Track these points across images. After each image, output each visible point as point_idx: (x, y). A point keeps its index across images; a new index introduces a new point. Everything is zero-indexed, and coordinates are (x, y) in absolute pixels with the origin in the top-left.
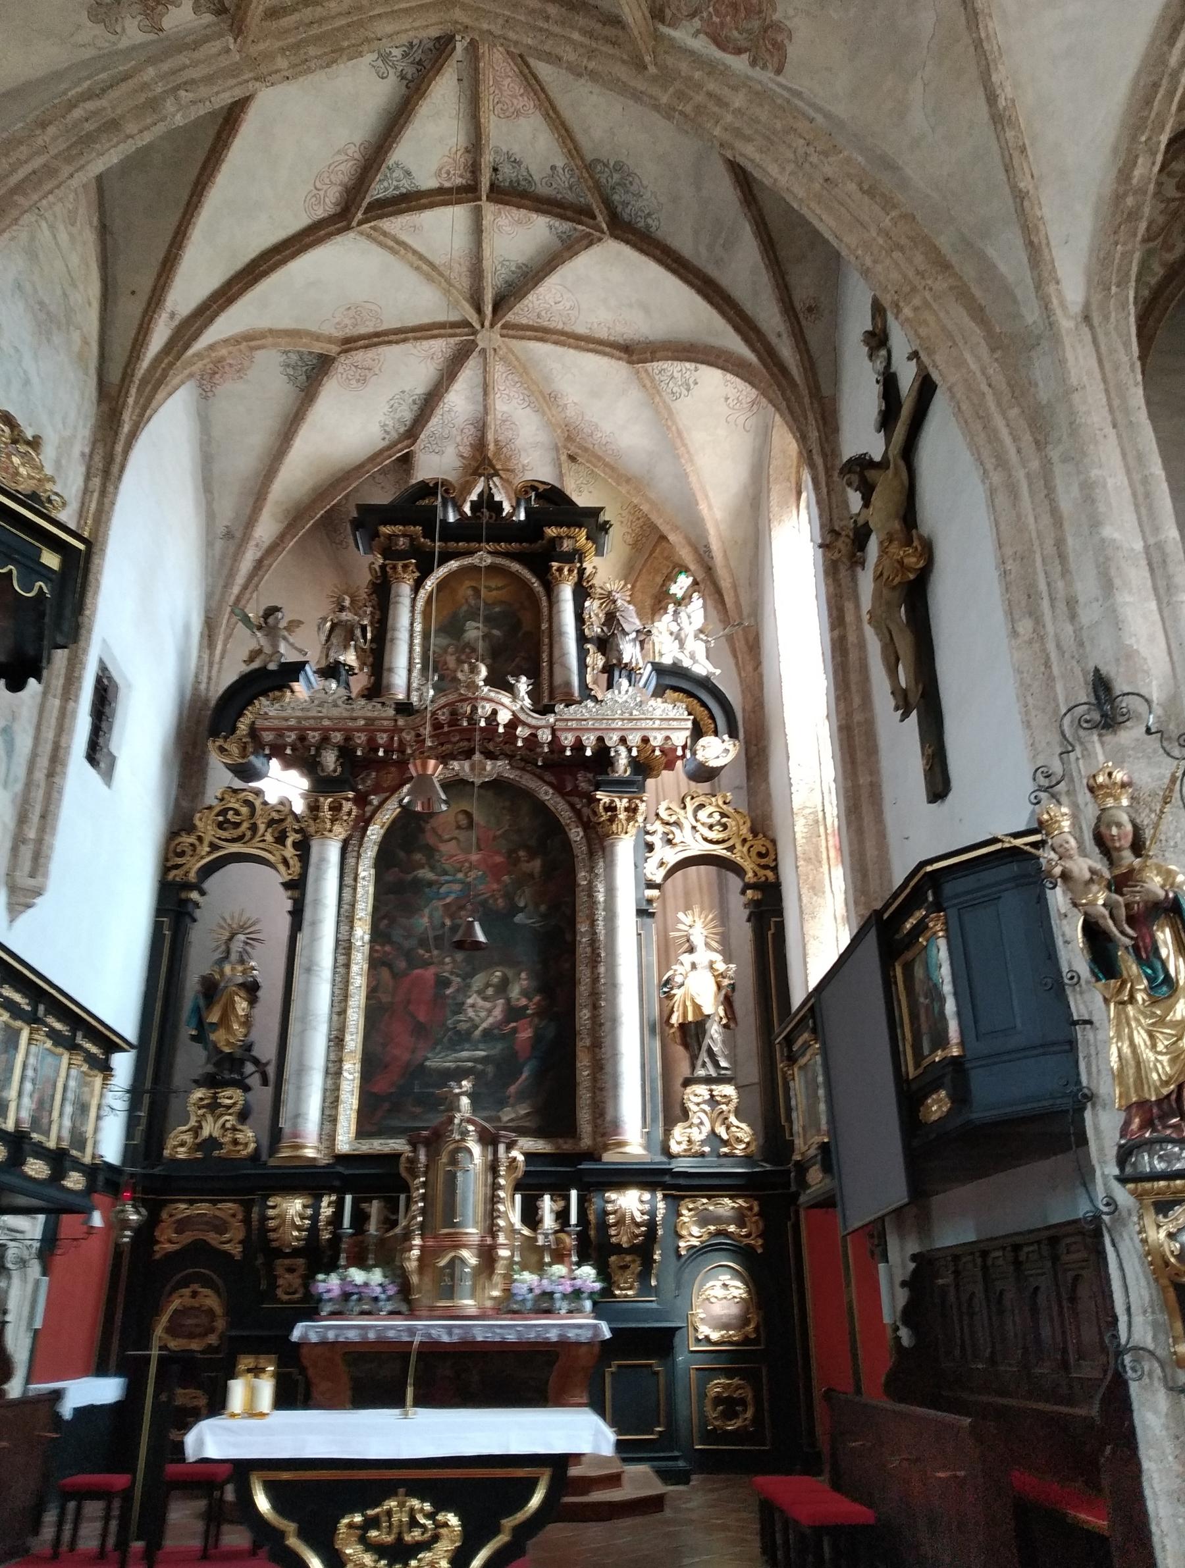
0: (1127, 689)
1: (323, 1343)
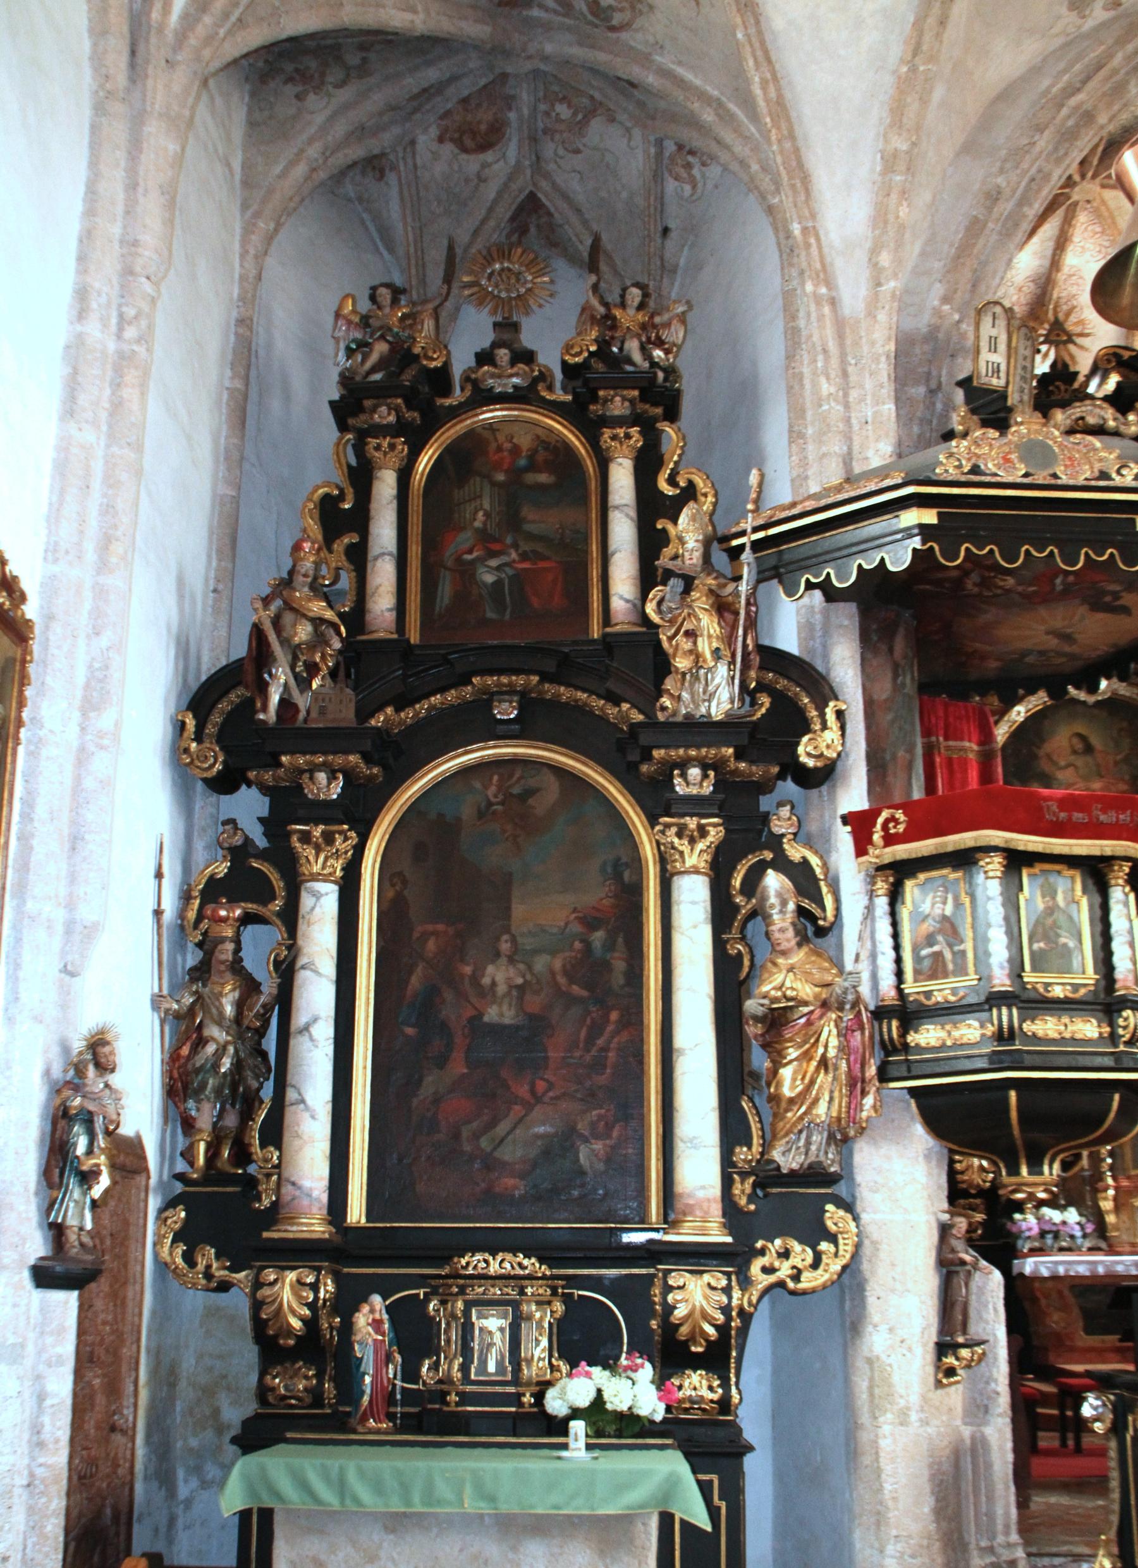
1: (1055, 1278)
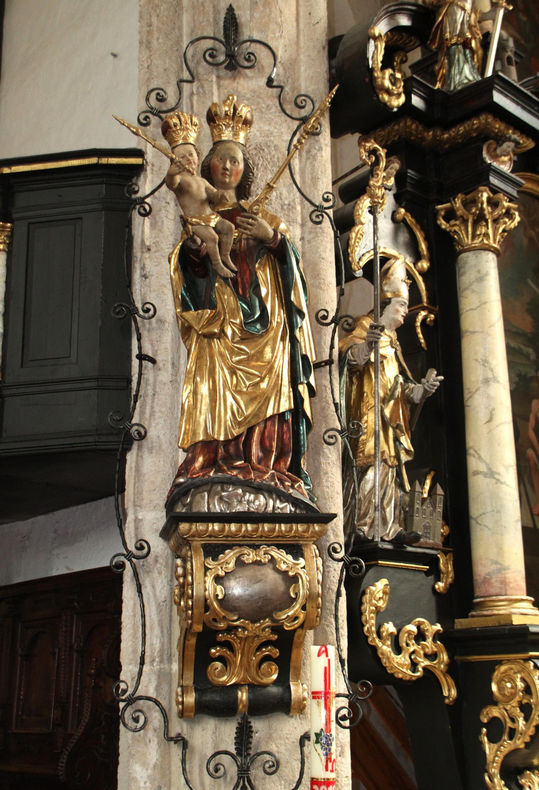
0: (256, 36)
